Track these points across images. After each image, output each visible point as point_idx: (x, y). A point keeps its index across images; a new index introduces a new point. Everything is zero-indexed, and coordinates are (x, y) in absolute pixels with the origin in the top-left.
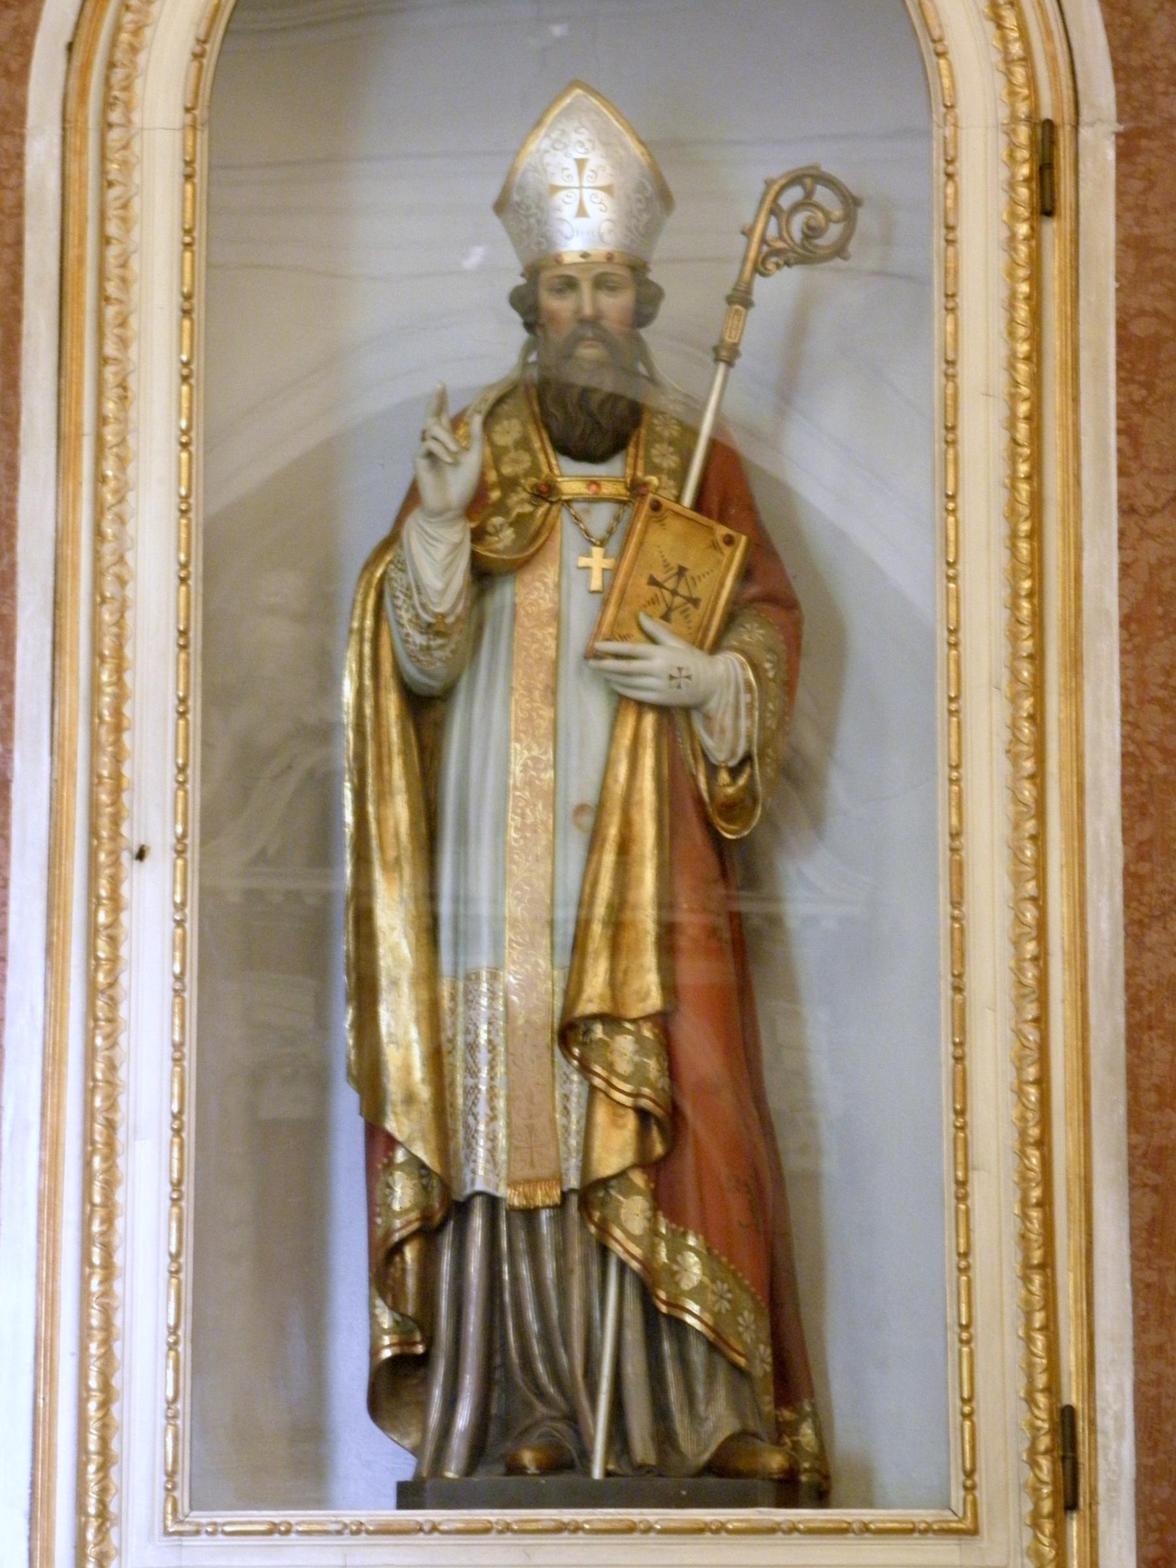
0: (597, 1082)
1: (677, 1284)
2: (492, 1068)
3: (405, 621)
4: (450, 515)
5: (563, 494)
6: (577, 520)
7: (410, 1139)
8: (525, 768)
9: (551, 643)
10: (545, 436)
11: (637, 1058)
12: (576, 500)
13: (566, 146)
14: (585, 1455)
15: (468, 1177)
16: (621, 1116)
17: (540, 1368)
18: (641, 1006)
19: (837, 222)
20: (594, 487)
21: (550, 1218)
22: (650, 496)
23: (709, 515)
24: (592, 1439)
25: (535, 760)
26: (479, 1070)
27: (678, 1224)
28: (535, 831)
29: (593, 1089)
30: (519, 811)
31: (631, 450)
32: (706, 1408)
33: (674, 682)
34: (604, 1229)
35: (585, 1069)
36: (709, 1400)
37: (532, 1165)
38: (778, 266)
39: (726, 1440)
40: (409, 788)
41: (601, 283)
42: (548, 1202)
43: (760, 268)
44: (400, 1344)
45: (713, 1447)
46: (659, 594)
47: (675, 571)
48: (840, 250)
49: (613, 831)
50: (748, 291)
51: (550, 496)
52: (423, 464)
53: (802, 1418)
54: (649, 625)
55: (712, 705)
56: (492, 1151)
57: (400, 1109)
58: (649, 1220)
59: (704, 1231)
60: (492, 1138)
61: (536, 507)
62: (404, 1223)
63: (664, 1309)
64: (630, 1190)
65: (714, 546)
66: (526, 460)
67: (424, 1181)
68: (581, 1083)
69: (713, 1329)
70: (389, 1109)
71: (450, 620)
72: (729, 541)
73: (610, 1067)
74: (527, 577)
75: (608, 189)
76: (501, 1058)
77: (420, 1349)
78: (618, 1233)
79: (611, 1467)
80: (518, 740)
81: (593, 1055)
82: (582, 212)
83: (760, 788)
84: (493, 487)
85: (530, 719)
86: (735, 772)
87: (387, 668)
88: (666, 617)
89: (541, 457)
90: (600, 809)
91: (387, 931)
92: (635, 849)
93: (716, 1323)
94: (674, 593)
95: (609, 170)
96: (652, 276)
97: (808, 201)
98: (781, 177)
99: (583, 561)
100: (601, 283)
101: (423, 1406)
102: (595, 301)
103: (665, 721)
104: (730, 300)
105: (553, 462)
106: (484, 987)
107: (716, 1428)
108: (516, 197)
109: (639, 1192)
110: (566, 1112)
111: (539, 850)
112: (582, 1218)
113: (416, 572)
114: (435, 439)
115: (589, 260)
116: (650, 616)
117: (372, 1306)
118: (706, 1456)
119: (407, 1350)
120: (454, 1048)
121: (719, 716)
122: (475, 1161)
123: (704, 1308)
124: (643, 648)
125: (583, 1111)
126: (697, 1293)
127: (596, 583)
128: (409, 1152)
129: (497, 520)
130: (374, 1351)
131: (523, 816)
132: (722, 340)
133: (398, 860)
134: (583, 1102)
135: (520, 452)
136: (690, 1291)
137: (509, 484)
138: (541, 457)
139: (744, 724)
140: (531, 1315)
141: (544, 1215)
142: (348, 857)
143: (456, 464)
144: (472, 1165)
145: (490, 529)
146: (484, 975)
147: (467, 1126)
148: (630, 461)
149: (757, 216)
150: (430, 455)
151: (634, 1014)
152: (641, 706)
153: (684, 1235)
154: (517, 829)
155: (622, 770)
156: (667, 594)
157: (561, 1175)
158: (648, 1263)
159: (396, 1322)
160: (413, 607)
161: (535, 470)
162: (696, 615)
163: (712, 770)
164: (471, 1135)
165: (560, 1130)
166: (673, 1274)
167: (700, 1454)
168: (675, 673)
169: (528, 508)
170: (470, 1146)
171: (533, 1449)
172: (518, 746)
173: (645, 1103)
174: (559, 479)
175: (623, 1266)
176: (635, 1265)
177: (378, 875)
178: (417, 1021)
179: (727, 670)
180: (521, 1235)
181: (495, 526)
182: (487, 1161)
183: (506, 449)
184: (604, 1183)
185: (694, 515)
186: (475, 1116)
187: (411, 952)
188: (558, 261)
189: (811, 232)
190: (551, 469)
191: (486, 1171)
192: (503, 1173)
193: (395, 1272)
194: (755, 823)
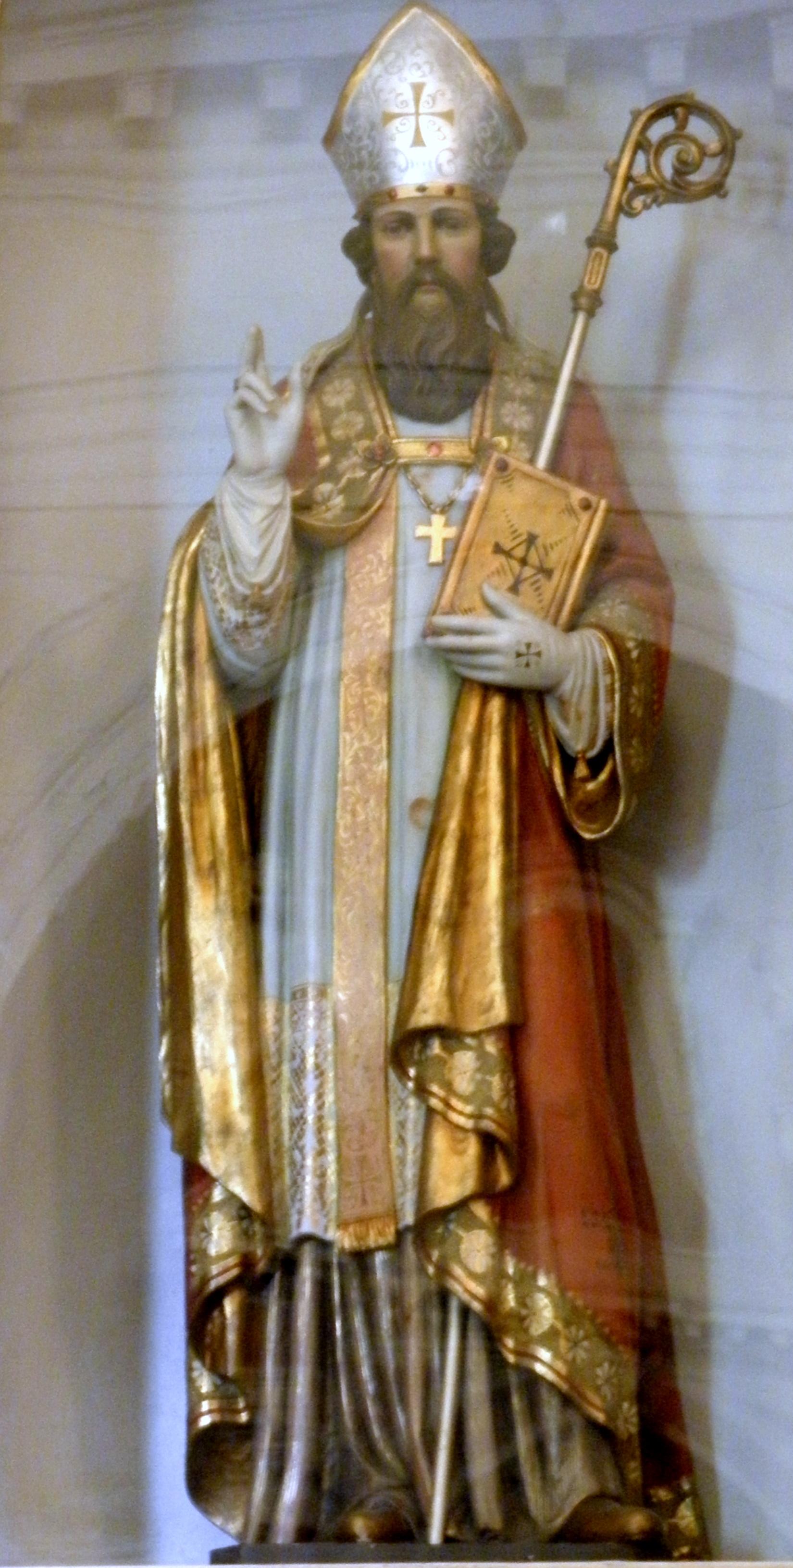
0: (434, 1102)
1: (526, 1330)
2: (320, 1096)
3: (219, 595)
4: (267, 473)
5: (399, 458)
6: (416, 486)
7: (228, 1174)
8: (356, 760)
9: (385, 619)
10: (381, 395)
11: (479, 1076)
12: (416, 465)
13: (400, 70)
14: (423, 1523)
15: (294, 1219)
16: (462, 1141)
17: (376, 1431)
18: (483, 1018)
19: (714, 155)
20: (434, 451)
21: (385, 1262)
22: (495, 456)
23: (565, 477)
24: (430, 1500)
25: (368, 751)
26: (305, 1099)
27: (528, 1261)
28: (367, 830)
29: (430, 1112)
30: (349, 808)
31: (478, 408)
32: (560, 1467)
33: (523, 660)
34: (443, 1271)
35: (422, 1091)
36: (564, 1458)
37: (364, 1201)
38: (646, 207)
39: (585, 1502)
40: (227, 785)
41: (440, 220)
42: (382, 1241)
43: (625, 209)
44: (220, 1410)
45: (567, 1511)
46: (505, 563)
47: (524, 537)
48: (717, 188)
49: (453, 825)
50: (613, 232)
51: (384, 459)
52: (236, 416)
53: (680, 1497)
54: (493, 596)
55: (567, 686)
56: (321, 1189)
57: (215, 1140)
58: (493, 1256)
59: (557, 1269)
60: (322, 1175)
61: (370, 472)
62: (221, 1269)
63: (511, 1358)
64: (472, 1223)
65: (570, 510)
66: (359, 421)
67: (245, 1224)
68: (418, 1108)
69: (567, 1379)
70: (204, 1141)
71: (269, 591)
72: (587, 506)
73: (448, 1086)
74: (359, 549)
75: (448, 116)
76: (330, 1085)
77: (244, 1417)
78: (458, 1271)
79: (451, 1532)
80: (348, 729)
81: (430, 1073)
82: (418, 141)
83: (622, 780)
84: (323, 452)
85: (361, 706)
86: (595, 765)
87: (202, 653)
88: (514, 589)
89: (377, 418)
90: (439, 805)
91: (202, 943)
92: (478, 848)
93: (570, 1371)
94: (524, 562)
95: (449, 95)
96: (504, 216)
97: (681, 133)
98: (647, 108)
99: (421, 531)
100: (440, 220)
101: (248, 1483)
102: (433, 240)
103: (514, 708)
104: (591, 243)
105: (389, 422)
106: (311, 1005)
107: (571, 1490)
108: (346, 129)
109: (481, 1226)
110: (402, 1140)
111: (372, 851)
112: (419, 1259)
113: (229, 538)
114: (249, 387)
115: (427, 193)
116: (496, 588)
117: (189, 1369)
118: (559, 1522)
119: (228, 1418)
120: (279, 1076)
121: (574, 699)
122: (301, 1200)
123: (557, 1354)
124: (485, 621)
125: (419, 1139)
126: (550, 1338)
127: (436, 555)
128: (226, 1190)
129: (325, 488)
130: (192, 1418)
131: (354, 813)
132: (581, 287)
133: (214, 865)
134: (420, 1128)
135: (353, 413)
136: (539, 1336)
137: (340, 449)
138: (377, 418)
139: (603, 707)
140: (365, 1372)
141: (379, 1258)
142: (162, 867)
143: (272, 415)
144: (297, 1205)
145: (319, 498)
146: (311, 993)
147: (293, 1163)
148: (477, 420)
149: (622, 151)
150: (244, 406)
151: (476, 1027)
152: (487, 689)
153: (534, 1277)
154: (346, 828)
155: (465, 758)
156: (516, 565)
157: (395, 1211)
158: (492, 1304)
159: (216, 1387)
160: (228, 579)
161: (369, 431)
162: (549, 587)
163: (569, 763)
164: (298, 1170)
165: (395, 1162)
166: (522, 1319)
167: (551, 1520)
168: (523, 649)
169: (360, 474)
170: (296, 1184)
171: (366, 1516)
172: (348, 737)
173: (488, 1125)
174: (395, 441)
175: (465, 1312)
176: (476, 1306)
177: (192, 883)
178: (235, 1042)
179: (583, 648)
180: (354, 1284)
181: (322, 494)
182: (315, 1200)
183: (337, 412)
184: (444, 1214)
185: (552, 479)
186: (301, 1150)
187: (227, 967)
188: (392, 195)
189: (683, 168)
190: (386, 428)
191: (314, 1212)
192: (333, 1214)
193: (212, 1328)
194: (617, 819)
